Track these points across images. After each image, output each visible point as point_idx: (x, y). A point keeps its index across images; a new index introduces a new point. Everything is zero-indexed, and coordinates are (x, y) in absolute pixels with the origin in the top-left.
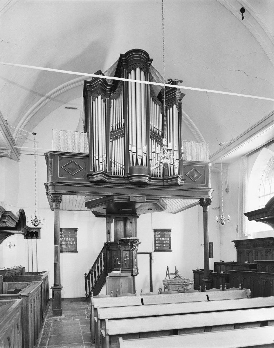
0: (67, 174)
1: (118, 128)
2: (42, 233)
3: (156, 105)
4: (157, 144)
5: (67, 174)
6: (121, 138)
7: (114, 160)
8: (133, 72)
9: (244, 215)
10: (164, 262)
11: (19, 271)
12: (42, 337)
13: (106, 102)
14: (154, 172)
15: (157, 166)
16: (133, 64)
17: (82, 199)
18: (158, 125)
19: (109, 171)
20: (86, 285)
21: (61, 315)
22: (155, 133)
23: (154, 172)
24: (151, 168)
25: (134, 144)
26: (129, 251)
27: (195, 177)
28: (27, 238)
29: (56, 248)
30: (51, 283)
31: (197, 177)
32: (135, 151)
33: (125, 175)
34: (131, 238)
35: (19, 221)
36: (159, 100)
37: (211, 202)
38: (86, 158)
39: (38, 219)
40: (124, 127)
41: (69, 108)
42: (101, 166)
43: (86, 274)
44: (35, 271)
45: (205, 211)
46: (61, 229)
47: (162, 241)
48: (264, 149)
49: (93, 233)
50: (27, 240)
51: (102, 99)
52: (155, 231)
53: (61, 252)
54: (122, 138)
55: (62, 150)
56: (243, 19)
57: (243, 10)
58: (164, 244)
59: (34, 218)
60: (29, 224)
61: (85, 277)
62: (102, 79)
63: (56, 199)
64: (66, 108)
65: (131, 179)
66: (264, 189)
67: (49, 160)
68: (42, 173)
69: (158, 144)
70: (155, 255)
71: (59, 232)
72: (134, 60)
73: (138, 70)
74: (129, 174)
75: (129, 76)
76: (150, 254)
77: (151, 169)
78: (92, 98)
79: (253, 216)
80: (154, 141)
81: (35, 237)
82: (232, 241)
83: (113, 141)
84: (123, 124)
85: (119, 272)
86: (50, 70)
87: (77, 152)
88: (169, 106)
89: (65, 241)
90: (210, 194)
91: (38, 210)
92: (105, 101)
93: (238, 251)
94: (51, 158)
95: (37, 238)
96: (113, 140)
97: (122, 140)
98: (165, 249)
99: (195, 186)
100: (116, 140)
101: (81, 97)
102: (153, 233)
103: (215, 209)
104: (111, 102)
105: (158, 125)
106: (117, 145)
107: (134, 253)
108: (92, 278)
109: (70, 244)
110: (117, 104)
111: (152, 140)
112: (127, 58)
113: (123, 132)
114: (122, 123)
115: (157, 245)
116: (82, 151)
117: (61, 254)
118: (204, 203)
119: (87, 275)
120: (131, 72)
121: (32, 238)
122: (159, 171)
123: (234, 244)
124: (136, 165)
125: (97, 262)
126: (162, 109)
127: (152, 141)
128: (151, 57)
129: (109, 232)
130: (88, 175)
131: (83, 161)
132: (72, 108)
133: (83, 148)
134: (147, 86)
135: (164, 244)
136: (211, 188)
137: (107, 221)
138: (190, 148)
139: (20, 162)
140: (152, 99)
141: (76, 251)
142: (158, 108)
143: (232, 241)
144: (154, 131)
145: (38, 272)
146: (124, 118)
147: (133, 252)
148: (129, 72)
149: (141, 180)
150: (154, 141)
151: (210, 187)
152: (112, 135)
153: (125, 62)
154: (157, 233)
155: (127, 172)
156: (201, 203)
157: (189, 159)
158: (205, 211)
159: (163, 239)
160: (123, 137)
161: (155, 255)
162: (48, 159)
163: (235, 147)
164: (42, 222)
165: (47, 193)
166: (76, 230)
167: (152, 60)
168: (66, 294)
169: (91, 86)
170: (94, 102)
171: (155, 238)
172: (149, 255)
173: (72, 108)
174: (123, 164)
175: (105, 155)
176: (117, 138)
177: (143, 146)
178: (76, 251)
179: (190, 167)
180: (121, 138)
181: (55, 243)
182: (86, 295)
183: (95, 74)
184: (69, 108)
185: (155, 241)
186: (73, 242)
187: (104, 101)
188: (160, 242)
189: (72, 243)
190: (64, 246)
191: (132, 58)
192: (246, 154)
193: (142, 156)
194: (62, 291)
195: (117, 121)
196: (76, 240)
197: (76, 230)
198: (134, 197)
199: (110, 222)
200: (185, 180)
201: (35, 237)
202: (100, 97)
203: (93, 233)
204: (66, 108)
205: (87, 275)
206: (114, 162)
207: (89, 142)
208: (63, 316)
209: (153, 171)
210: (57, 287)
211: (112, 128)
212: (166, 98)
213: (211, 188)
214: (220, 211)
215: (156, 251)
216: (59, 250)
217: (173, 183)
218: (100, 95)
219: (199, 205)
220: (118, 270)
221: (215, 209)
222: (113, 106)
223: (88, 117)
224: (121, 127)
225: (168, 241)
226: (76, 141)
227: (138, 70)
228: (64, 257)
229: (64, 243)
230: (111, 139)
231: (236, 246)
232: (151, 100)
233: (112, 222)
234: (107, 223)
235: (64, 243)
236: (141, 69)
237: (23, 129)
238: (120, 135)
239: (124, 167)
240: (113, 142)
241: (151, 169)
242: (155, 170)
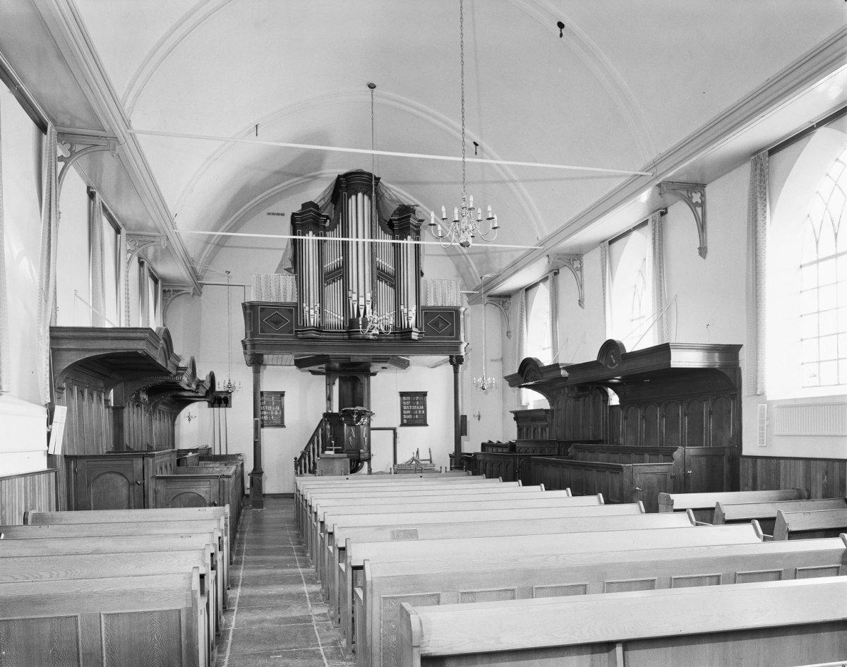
0: (269, 329)
2: (235, 399)
5: (269, 329)
8: (353, 197)
10: (416, 442)
11: (205, 452)
17: (290, 358)
21: (262, 508)
25: (355, 290)
26: (354, 425)
28: (212, 406)
29: (256, 423)
30: (249, 467)
32: (356, 299)
34: (356, 408)
35: (210, 388)
38: (294, 310)
39: (232, 383)
41: (274, 214)
42: (312, 320)
43: (296, 459)
44: (223, 453)
45: (456, 372)
46: (262, 393)
47: (414, 408)
48: (822, 130)
49: (306, 398)
50: (212, 409)
52: (402, 394)
53: (263, 426)
55: (263, 300)
56: (561, 35)
57: (561, 25)
58: (415, 415)
59: (227, 383)
60: (220, 387)
63: (256, 362)
64: (269, 214)
66: (817, 243)
67: (248, 311)
68: (238, 326)
70: (402, 431)
71: (259, 398)
72: (352, 183)
76: (394, 430)
81: (223, 404)
82: (511, 412)
85: (332, 453)
87: (282, 301)
89: (268, 410)
91: (233, 373)
93: (518, 426)
94: (251, 309)
95: (226, 406)
96: (328, 284)
97: (340, 283)
98: (417, 422)
101: (244, 597)
102: (399, 398)
103: (496, 360)
107: (364, 430)
108: (305, 464)
109: (274, 415)
113: (341, 273)
115: (405, 416)
116: (289, 300)
117: (262, 429)
118: (457, 361)
121: (219, 406)
123: (513, 415)
129: (329, 399)
130: (296, 331)
132: (278, 214)
133: (290, 297)
135: (415, 415)
137: (326, 382)
138: (432, 288)
139: (202, 298)
141: (282, 425)
143: (511, 412)
145: (229, 454)
147: (361, 426)
152: (327, 277)
154: (404, 398)
157: (431, 303)
158: (456, 372)
159: (415, 407)
161: (402, 431)
162: (246, 310)
163: (684, 159)
164: (237, 389)
165: (245, 353)
166: (282, 394)
168: (269, 487)
171: (402, 405)
172: (392, 431)
173: (278, 214)
176: (334, 281)
177: (366, 291)
178: (282, 425)
179: (434, 314)
181: (255, 416)
184: (274, 214)
185: (402, 409)
186: (278, 412)
188: (409, 412)
189: (276, 413)
190: (266, 418)
191: (353, 181)
192: (767, 147)
194: (263, 476)
195: (332, 262)
196: (282, 409)
197: (282, 394)
199: (331, 383)
201: (223, 404)
203: (306, 398)
204: (269, 214)
207: (297, 284)
208: (264, 509)
210: (258, 471)
212: (401, 222)
214: (503, 364)
215: (403, 425)
216: (260, 423)
219: (325, 412)
220: (331, 450)
221: (496, 360)
225: (421, 410)
227: (360, 195)
228: (266, 433)
229: (265, 413)
231: (515, 419)
233: (334, 384)
234: (327, 385)
235: (265, 413)
236: (364, 194)
237: (309, 593)
239: (342, 318)
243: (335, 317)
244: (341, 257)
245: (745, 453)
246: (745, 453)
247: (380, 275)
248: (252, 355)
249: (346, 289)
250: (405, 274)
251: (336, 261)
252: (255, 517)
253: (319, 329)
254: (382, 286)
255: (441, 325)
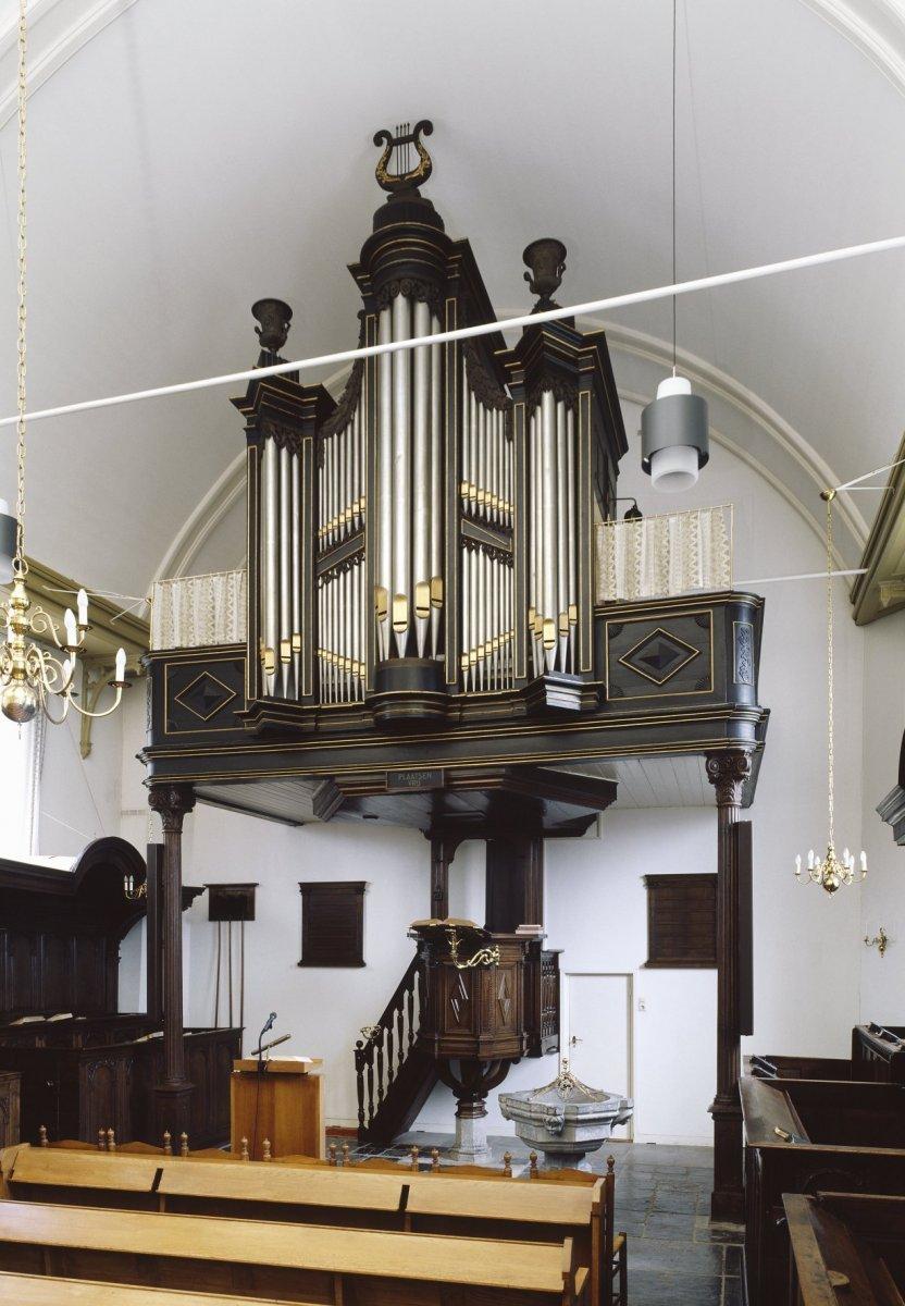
1: (349, 530)
12: (722, 1248)
20: (360, 1080)
43: (359, 1044)
61: (358, 1053)
86: (483, 332)
96: (328, 579)
100: (338, 578)
111: (470, 552)
119: (362, 1048)
122: (505, 663)
125: (396, 1002)
126: (509, 422)
131: (616, 631)
149: (404, 713)
155: (586, 666)
172: (624, 980)
182: (359, 1115)
183: (535, 312)
191: (392, 257)
198: (400, 776)
205: (362, 1048)
211: (330, 534)
223: (379, 494)
226: (219, 604)
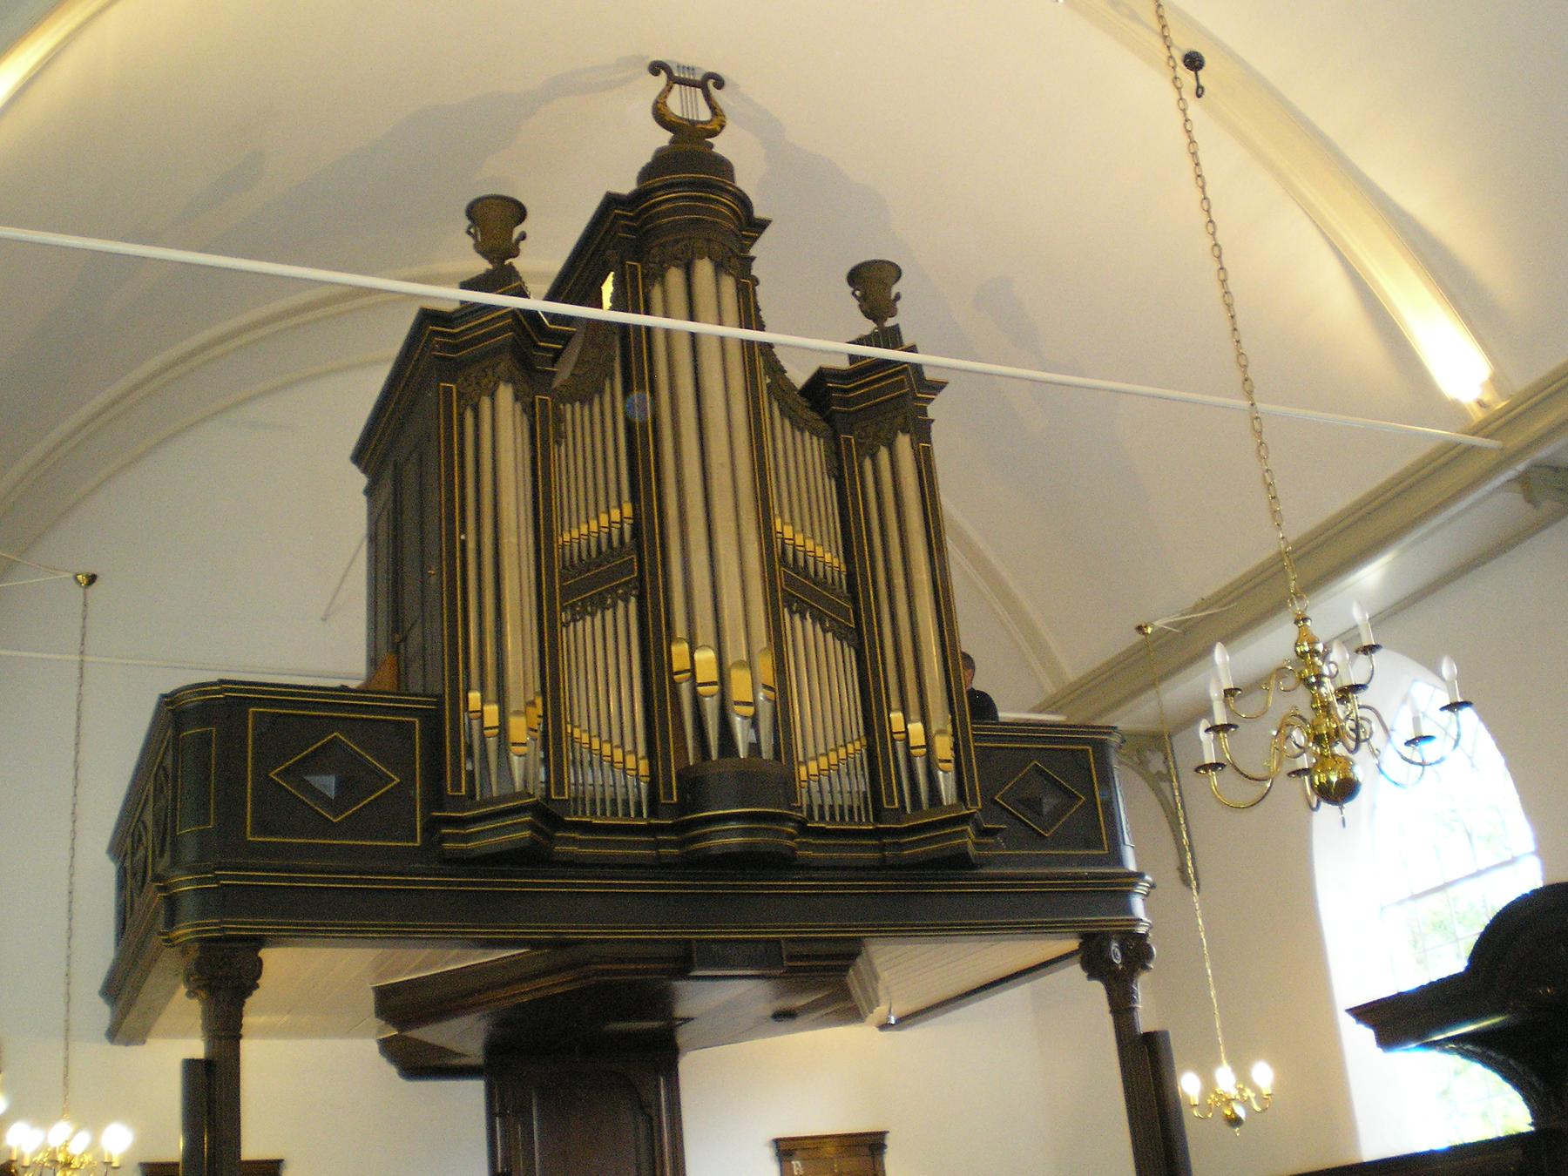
1: (604, 548)
3: (798, 434)
4: (825, 631)
6: (621, 604)
7: (585, 727)
8: (675, 277)
9: (1359, 1039)
13: (534, 416)
14: (820, 791)
15: (834, 760)
16: (677, 241)
18: (797, 520)
19: (560, 791)
22: (807, 577)
23: (820, 791)
24: (803, 770)
27: (1046, 810)
31: (1057, 814)
33: (653, 813)
36: (812, 408)
37: (1148, 955)
40: (639, 547)
51: (516, 398)
54: (627, 601)
62: (516, 314)
65: (705, 837)
69: (829, 635)
73: (704, 269)
74: (683, 807)
75: (656, 293)
77: (804, 776)
78: (461, 395)
79: (1398, 1020)
80: (803, 618)
83: (575, 621)
84: (627, 527)
88: (868, 441)
90: (1138, 906)
92: (529, 409)
99: (1038, 861)
104: (560, 419)
105: (797, 520)
106: (603, 647)
110: (595, 430)
111: (792, 613)
112: (640, 214)
113: (629, 574)
114: (621, 522)
118: (1115, 960)
120: (663, 277)
124: (721, 753)
127: (797, 617)
128: (759, 213)
134: (748, 346)
136: (1140, 875)
140: (775, 405)
142: (812, 450)
144: (801, 563)
146: (634, 498)
148: (659, 276)
150: (803, 618)
151: (1132, 866)
152: (570, 586)
153: (629, 229)
156: (1093, 960)
160: (633, 600)
162: (178, 728)
167: (762, 225)
169: (453, 336)
170: (469, 415)
174: (641, 750)
175: (539, 701)
176: (600, 603)
180: (621, 604)
187: (524, 410)
191: (665, 214)
193: (753, 704)
195: (597, 520)
198: (715, 948)
200: (999, 830)
202: (505, 394)
206: (585, 738)
209: (814, 786)
213: (1140, 875)
217: (627, 856)
218: (507, 382)
222: (570, 438)
224: (616, 543)
227: (704, 269)
230: (564, 609)
232: (772, 413)
238: (614, 589)
239: (644, 767)
240: (580, 624)
241: (804, 776)
242: (824, 780)
243: (613, 756)
244: (628, 510)
245: (473, 1092)
246: (473, 1092)
247: (790, 587)
248: (207, 944)
249: (653, 640)
250: (899, 581)
251: (584, 530)
252: (67, 1165)
253: (547, 814)
254: (803, 632)
255: (1049, 803)
